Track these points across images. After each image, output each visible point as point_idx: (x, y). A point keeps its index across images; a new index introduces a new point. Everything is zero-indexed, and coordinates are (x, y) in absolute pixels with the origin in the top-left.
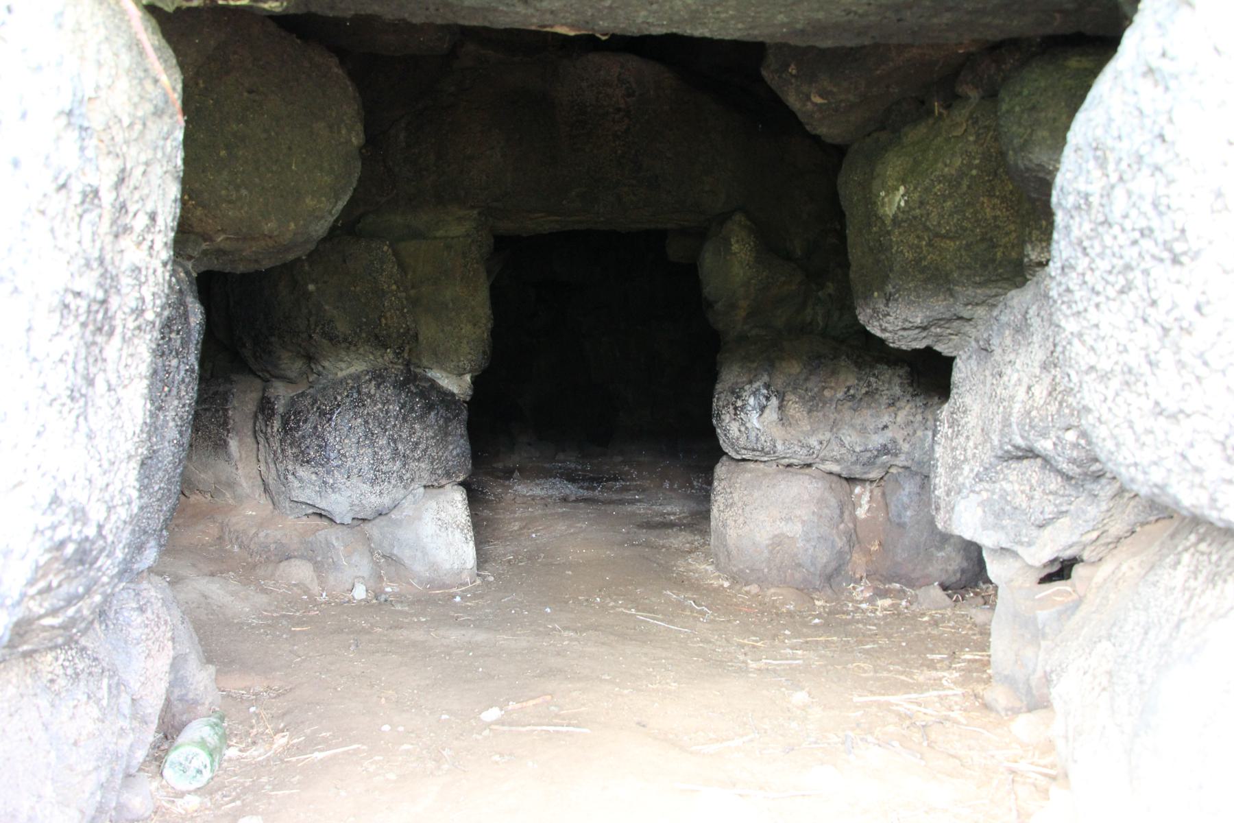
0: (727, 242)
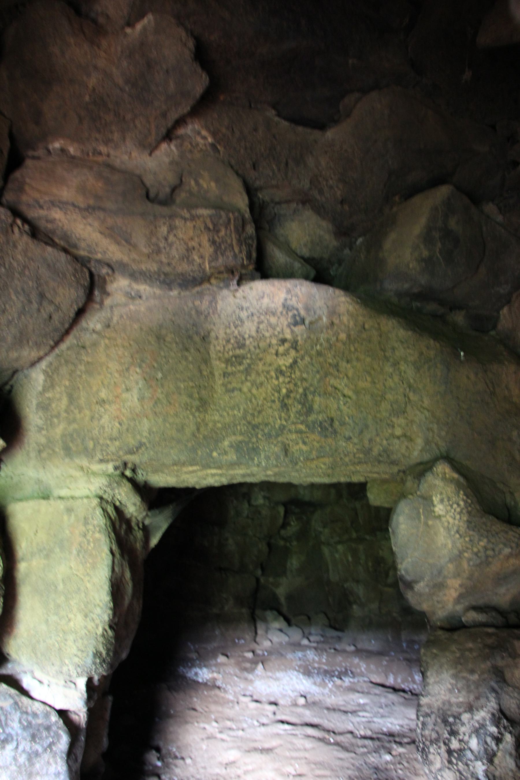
0: (427, 500)
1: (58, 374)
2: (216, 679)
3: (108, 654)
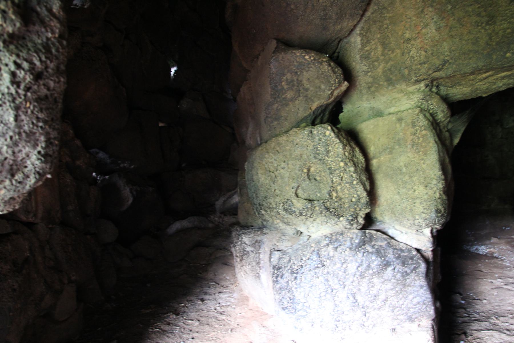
1: (370, 32)
2: (493, 253)
3: (445, 212)
